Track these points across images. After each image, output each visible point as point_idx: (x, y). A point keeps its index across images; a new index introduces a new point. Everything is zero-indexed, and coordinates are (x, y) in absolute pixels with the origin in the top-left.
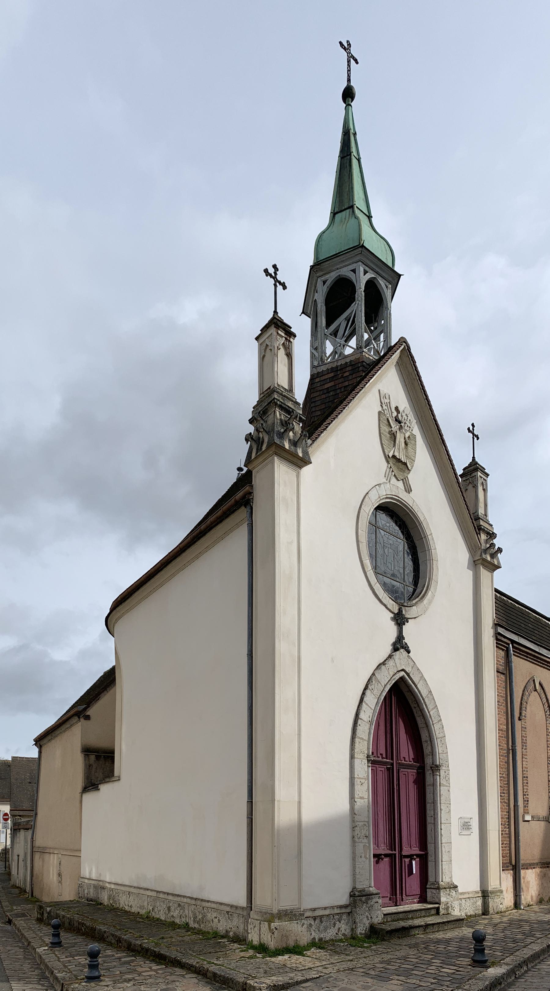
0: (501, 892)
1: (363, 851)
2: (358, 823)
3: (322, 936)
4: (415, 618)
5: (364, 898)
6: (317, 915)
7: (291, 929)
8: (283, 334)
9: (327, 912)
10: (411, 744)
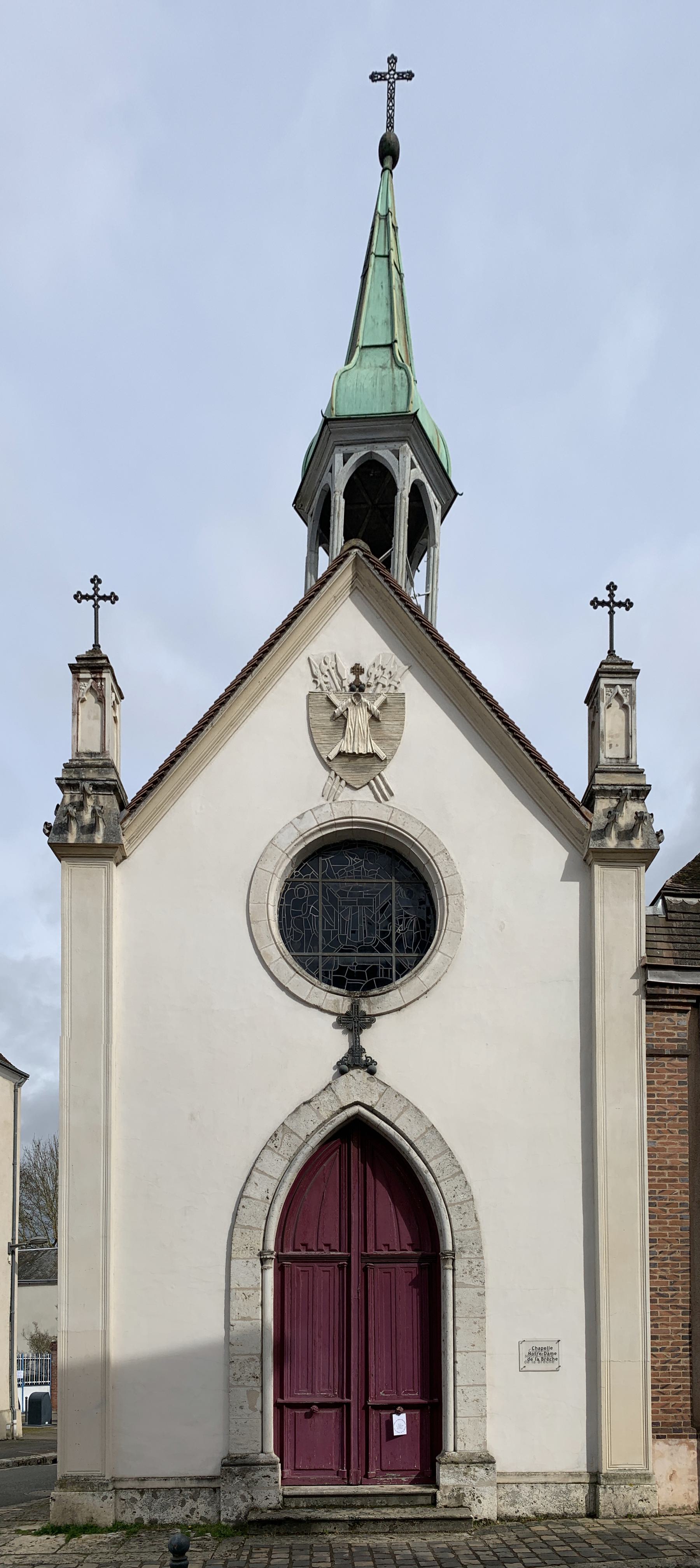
0: (647, 1477)
1: (246, 1399)
2: (236, 1357)
3: (156, 1516)
4: (399, 1009)
5: (237, 1468)
6: (149, 1487)
7: (80, 1502)
8: (88, 676)
9: (170, 1484)
10: (405, 1220)
